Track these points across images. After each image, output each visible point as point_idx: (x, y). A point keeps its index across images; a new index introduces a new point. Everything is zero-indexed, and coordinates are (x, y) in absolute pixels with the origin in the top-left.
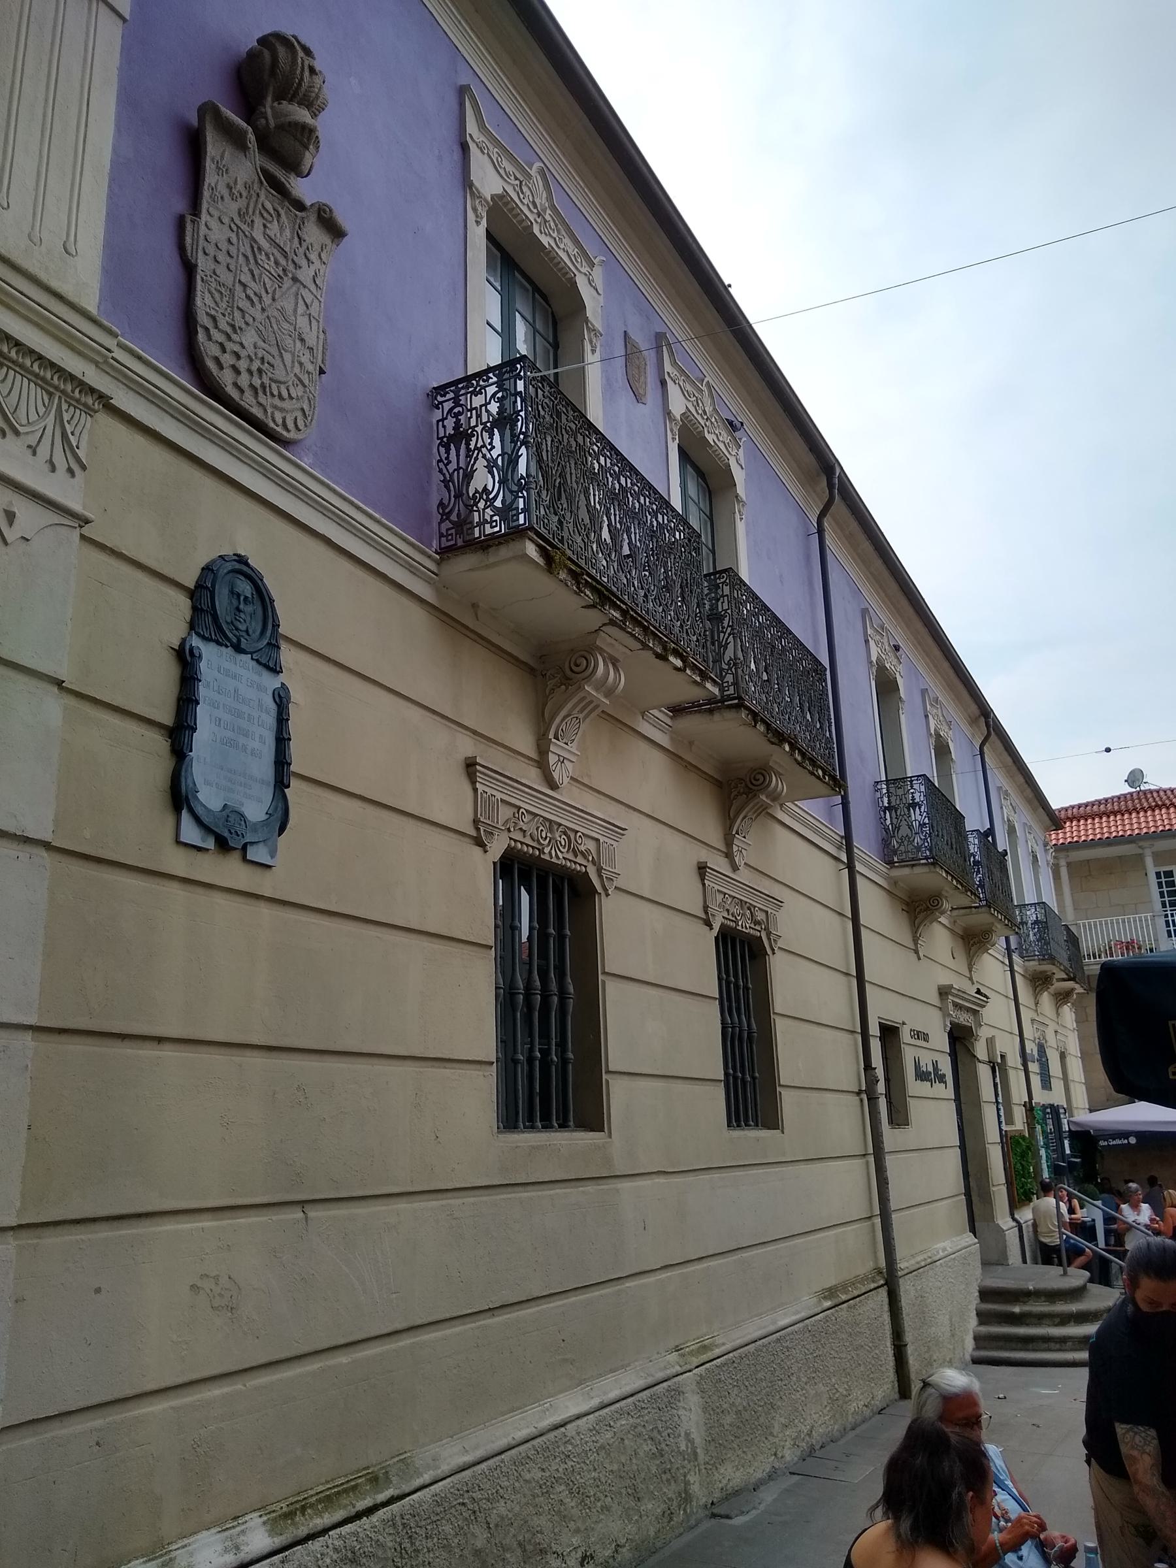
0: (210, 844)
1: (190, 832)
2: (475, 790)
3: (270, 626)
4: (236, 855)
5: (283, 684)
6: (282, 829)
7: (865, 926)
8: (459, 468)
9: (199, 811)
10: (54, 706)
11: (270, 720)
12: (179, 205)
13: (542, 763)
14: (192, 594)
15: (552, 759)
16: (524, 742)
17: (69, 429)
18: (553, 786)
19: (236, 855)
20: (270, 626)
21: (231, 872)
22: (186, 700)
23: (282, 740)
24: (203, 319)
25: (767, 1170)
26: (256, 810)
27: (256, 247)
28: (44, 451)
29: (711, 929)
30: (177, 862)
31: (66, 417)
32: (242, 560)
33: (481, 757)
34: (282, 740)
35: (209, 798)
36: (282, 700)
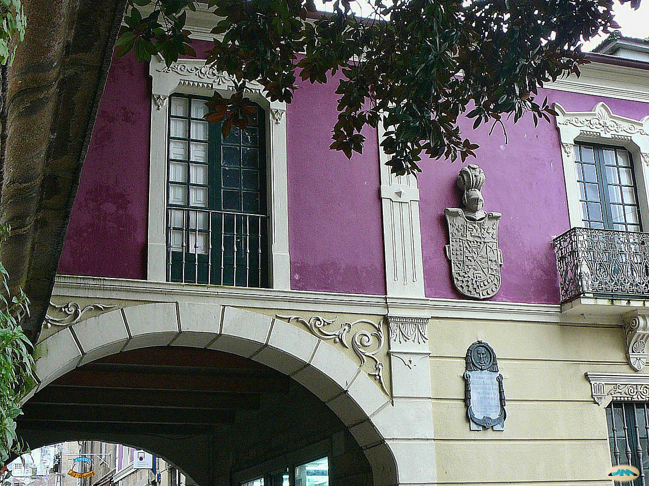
0: (481, 428)
1: (474, 427)
2: (591, 384)
3: (492, 359)
4: (490, 429)
5: (500, 374)
6: (505, 419)
7: (294, 373)
8: (564, 270)
9: (475, 420)
10: (429, 404)
11: (497, 387)
12: (441, 239)
13: (628, 363)
14: (465, 358)
15: (632, 360)
16: (619, 357)
17: (421, 331)
18: (636, 371)
19: (490, 429)
20: (492, 359)
21: (490, 434)
22: (467, 391)
23: (501, 392)
24: (455, 275)
25: (455, 360)
26: (495, 415)
27: (469, 242)
28: (416, 340)
29: (500, 374)
30: (473, 435)
31: (420, 328)
32: (479, 342)
33: (589, 372)
34: (501, 392)
35: (478, 415)
36: (500, 380)
